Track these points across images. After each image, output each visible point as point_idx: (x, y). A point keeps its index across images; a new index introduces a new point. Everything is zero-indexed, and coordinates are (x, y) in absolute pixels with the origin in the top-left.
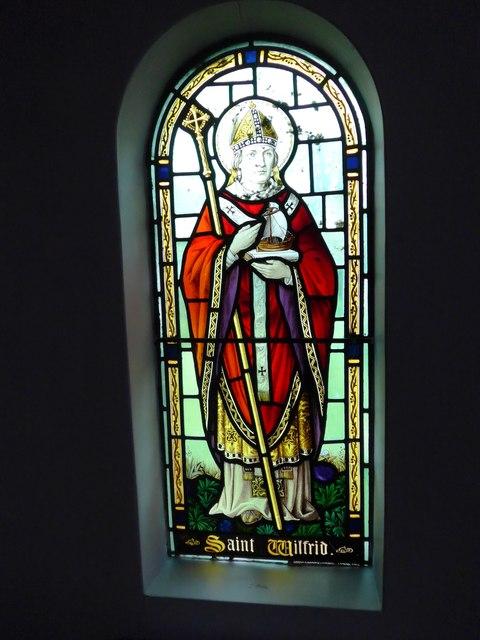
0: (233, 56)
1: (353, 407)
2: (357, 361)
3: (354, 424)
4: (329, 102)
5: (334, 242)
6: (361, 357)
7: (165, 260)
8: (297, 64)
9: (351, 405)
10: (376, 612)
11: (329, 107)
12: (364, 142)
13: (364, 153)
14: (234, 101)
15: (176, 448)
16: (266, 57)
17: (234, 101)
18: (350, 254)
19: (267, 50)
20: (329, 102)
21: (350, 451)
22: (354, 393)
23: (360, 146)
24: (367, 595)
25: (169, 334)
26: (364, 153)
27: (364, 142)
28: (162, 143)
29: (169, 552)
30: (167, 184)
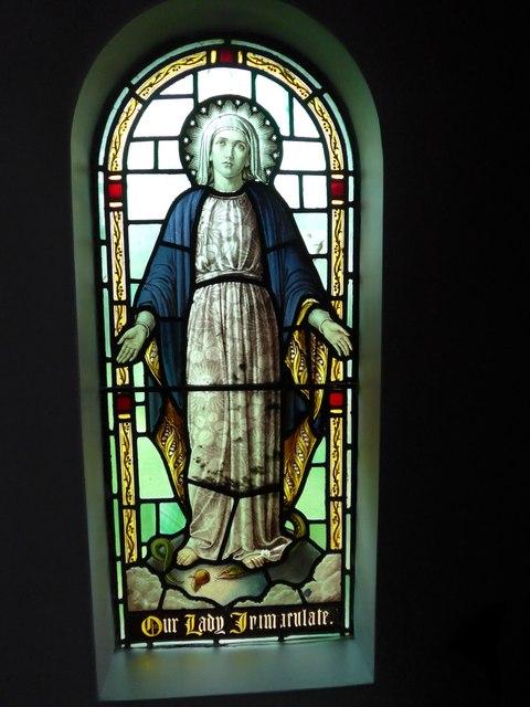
0: (204, 53)
1: (336, 462)
2: (340, 411)
3: (337, 278)
4: (322, 139)
5: (313, 232)
6: (344, 407)
7: (116, 298)
8: (338, 258)
9: (333, 527)
10: (367, 686)
11: (320, 145)
12: (351, 168)
13: (351, 179)
14: (191, 76)
15: (129, 522)
16: (245, 59)
17: (191, 76)
18: (304, 98)
19: (245, 50)
20: (322, 139)
21: (332, 510)
22: (336, 481)
23: (346, 172)
24: (354, 665)
25: (119, 382)
26: (351, 179)
27: (351, 168)
28: (113, 151)
29: (119, 641)
30: (120, 204)
